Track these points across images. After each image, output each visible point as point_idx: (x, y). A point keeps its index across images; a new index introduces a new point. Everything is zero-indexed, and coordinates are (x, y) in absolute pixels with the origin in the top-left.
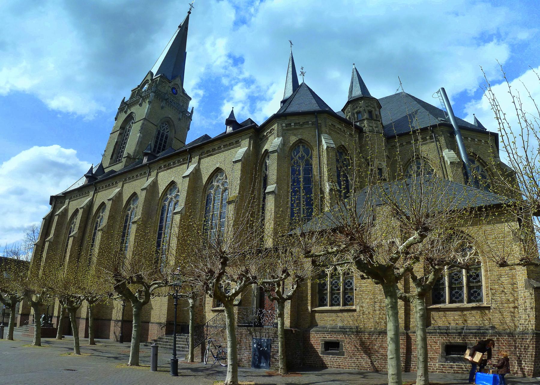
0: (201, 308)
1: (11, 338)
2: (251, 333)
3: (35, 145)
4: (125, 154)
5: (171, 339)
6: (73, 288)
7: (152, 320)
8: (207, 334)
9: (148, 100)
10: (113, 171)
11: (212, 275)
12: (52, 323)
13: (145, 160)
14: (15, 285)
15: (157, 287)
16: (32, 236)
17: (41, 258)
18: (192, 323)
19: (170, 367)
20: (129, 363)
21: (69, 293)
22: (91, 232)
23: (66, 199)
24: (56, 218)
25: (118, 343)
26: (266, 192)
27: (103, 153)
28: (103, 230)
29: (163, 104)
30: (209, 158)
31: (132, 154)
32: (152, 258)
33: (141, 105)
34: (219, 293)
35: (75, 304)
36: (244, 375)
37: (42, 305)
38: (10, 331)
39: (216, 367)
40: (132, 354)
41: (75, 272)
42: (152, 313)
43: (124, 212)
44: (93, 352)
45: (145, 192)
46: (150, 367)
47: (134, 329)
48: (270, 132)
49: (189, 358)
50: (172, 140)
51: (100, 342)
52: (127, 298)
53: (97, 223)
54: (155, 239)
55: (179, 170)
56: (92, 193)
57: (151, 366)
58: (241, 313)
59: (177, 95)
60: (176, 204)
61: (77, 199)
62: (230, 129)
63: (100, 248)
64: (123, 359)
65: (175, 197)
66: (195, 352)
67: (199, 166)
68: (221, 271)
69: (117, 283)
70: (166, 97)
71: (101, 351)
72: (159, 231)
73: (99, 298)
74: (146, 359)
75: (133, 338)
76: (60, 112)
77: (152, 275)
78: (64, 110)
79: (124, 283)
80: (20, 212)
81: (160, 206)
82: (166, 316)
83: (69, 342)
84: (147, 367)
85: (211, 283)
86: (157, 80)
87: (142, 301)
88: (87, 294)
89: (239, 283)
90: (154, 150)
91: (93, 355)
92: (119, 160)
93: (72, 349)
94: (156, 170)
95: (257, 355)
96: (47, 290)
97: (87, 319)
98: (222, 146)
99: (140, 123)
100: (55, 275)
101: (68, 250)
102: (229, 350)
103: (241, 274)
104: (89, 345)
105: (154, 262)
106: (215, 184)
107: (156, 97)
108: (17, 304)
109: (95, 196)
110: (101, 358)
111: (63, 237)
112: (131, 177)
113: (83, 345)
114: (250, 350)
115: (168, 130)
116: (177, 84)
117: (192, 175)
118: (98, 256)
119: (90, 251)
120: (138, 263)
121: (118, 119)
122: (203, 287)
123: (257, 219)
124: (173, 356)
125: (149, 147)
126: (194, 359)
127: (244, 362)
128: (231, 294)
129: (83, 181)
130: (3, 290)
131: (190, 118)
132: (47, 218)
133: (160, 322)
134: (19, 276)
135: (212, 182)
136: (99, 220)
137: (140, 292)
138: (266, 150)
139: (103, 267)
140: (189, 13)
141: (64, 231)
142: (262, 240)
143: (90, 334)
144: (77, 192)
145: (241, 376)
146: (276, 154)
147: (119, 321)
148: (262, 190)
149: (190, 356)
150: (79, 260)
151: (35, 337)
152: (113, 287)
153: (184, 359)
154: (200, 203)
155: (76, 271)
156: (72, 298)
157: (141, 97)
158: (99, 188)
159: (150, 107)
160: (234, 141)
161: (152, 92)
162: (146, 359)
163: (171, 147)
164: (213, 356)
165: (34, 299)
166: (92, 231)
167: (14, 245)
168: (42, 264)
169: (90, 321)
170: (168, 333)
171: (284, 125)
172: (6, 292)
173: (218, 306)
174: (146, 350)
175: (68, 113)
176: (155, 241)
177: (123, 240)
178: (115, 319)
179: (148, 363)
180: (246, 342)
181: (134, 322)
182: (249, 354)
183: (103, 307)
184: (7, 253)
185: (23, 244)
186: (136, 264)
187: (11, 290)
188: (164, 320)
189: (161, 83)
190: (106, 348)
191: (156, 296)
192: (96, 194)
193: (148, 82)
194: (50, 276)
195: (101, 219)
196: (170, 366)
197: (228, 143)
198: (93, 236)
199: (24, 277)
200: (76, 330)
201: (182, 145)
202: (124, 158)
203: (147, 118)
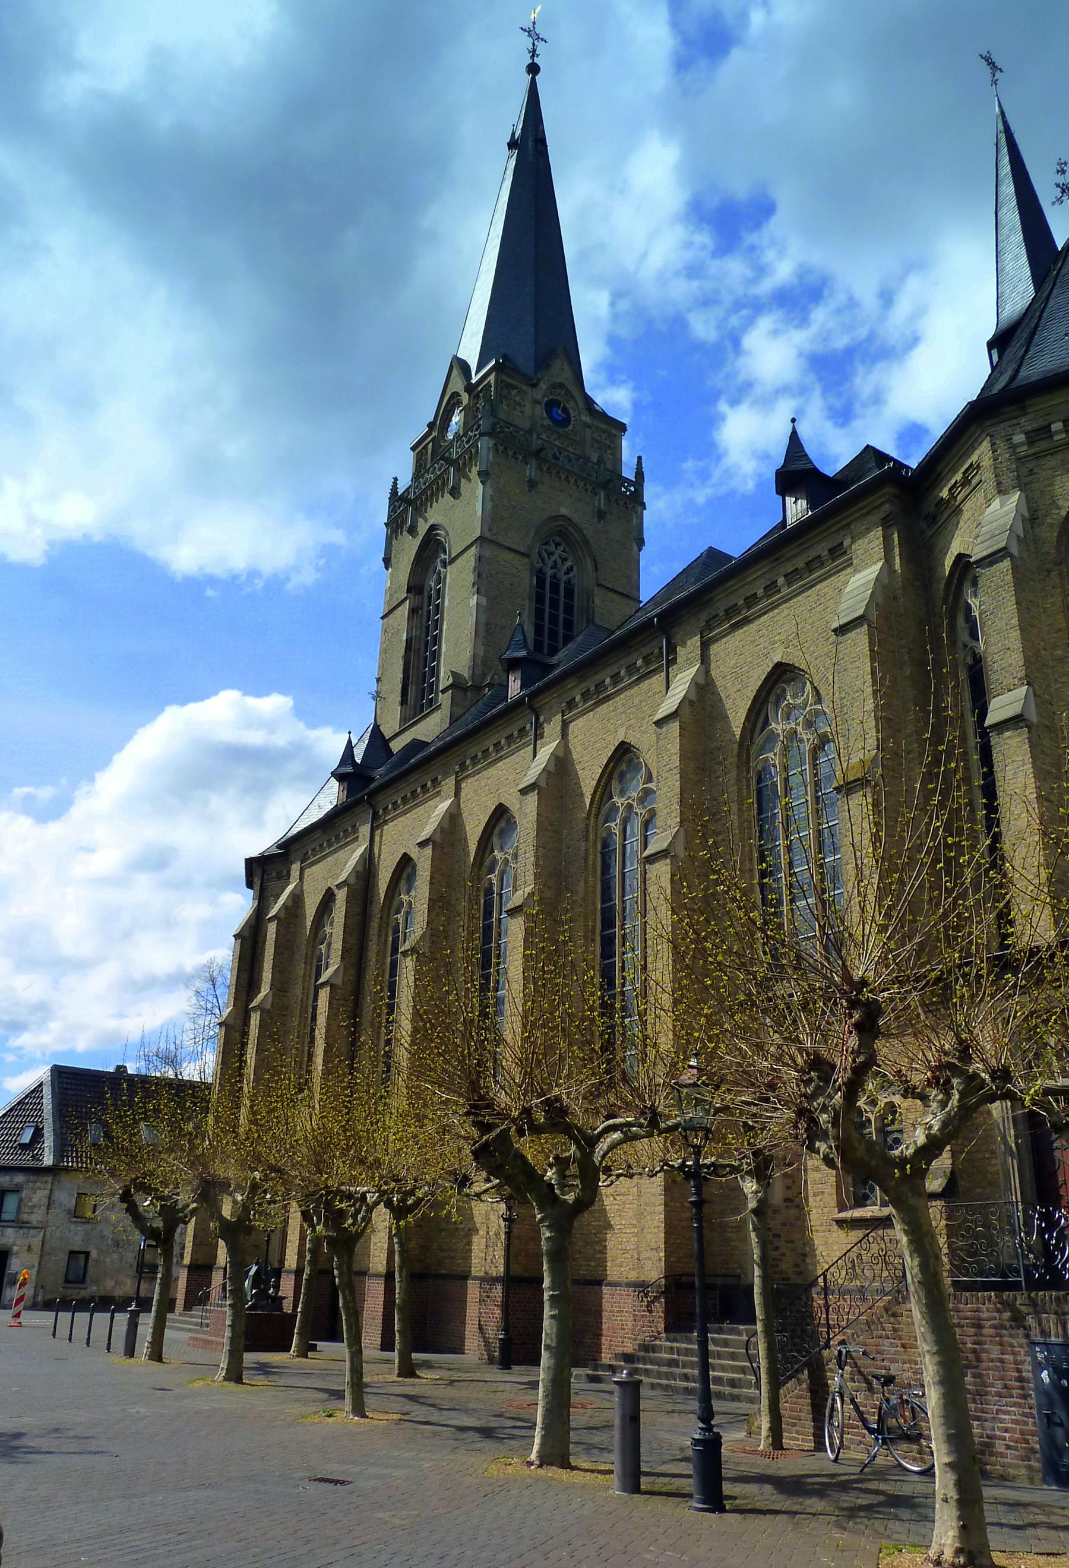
0: (793, 1212)
1: (156, 1355)
2: (1018, 1320)
3: (170, 702)
4: (444, 680)
5: (687, 1352)
6: (341, 1165)
7: (613, 1272)
8: (829, 1327)
9: (475, 470)
10: (417, 745)
11: (826, 1078)
12: (280, 1294)
13: (515, 687)
14: (174, 1165)
15: (621, 1142)
16: (210, 998)
17: (241, 1068)
18: (764, 1278)
19: (689, 1476)
20: (533, 1456)
21: (330, 1183)
22: (381, 962)
23: (292, 863)
24: (272, 928)
25: (495, 1369)
26: (988, 723)
27: (374, 687)
28: (418, 953)
29: (530, 471)
30: (740, 633)
31: (466, 674)
32: (592, 1034)
33: (455, 493)
34: (861, 1151)
35: (350, 1221)
36: (1012, 1519)
37: (250, 1230)
38: (155, 1328)
39: (881, 1474)
40: (545, 1417)
41: (346, 1107)
42: (610, 1244)
43: (477, 878)
44: (407, 1408)
45: (533, 798)
46: (611, 1472)
47: (547, 1312)
48: (966, 481)
49: (764, 1432)
50: (589, 596)
51: (432, 1367)
52: (517, 1189)
53: (396, 930)
54: (593, 960)
55: (636, 701)
56: (365, 830)
57: (616, 1467)
58: (959, 1226)
59: (571, 427)
60: (647, 825)
61: (324, 857)
62: (797, 509)
63: (416, 1014)
64: (512, 1437)
65: (642, 801)
66: (784, 1406)
67: (707, 672)
68: (861, 1059)
69: (481, 1137)
70: (536, 443)
71: (436, 1402)
72: (603, 930)
73: (426, 1194)
74: (597, 1438)
75: (548, 1347)
76: (211, 581)
77: (599, 1095)
78: (219, 571)
79: (504, 1136)
80: (168, 923)
81: (595, 841)
82: (662, 1254)
83: (331, 1365)
84: (600, 1472)
85: (824, 1109)
86: (489, 385)
87: (570, 1197)
88: (386, 1183)
89: (939, 1102)
90: (538, 645)
91: (406, 1417)
92: (431, 702)
93: (339, 1395)
94: (557, 713)
95: (1061, 1425)
96: (266, 1175)
97: (389, 1277)
98: (781, 581)
99: (469, 560)
100: (287, 1124)
101: (317, 1031)
102: (933, 1399)
103: (941, 1067)
104: (395, 1378)
105: (601, 1048)
106: (778, 727)
107: (501, 448)
108: (178, 1230)
109: (377, 838)
110: (435, 1434)
111: (298, 991)
112: (480, 754)
113: (375, 1379)
114: (1025, 1397)
115: (569, 564)
116: (561, 385)
117: (687, 709)
118: (413, 1043)
119: (386, 1027)
120: (545, 1055)
121: (393, 560)
122: (796, 1127)
123: (974, 837)
124: (701, 1425)
125: (519, 637)
126: (785, 1434)
127: (1003, 1455)
128: (911, 1151)
129: (331, 796)
130: (140, 1183)
131: (636, 501)
132: (246, 934)
133: (642, 1278)
134: (184, 1135)
135: (766, 723)
136: (400, 917)
137: (561, 1163)
138: (960, 557)
139: (430, 1082)
140: (533, 69)
141: (300, 968)
142: (1004, 918)
143: (397, 1335)
144: (318, 834)
145: (1001, 1525)
146: (1006, 563)
147: (494, 1280)
148: (971, 719)
149: (765, 1423)
150: (353, 1063)
151: (227, 1348)
152: (467, 1151)
153: (743, 1435)
154: (734, 808)
155: (349, 1102)
156: (341, 1202)
157: (450, 462)
158: (385, 809)
159: (490, 491)
160: (822, 549)
161: (481, 435)
162: (597, 1438)
163: (590, 621)
164: (864, 1421)
165: (227, 1211)
166: (385, 956)
167: (164, 1034)
168: (245, 1089)
169: (397, 1285)
170: (676, 1324)
171: (1019, 438)
172: (147, 1190)
173: (861, 1201)
174: (597, 1400)
175: (235, 577)
176: (593, 968)
177: (486, 978)
178: (482, 1274)
179: (606, 1455)
180: (1002, 1361)
181: (546, 1284)
182: (1024, 1414)
183: (441, 1230)
184: (148, 1059)
185: (189, 1025)
186: (539, 1062)
187: (161, 1182)
188: (654, 1271)
189: (504, 392)
190: (451, 1392)
191: (621, 1175)
192: (378, 832)
193: (459, 403)
194: (270, 1129)
195: (408, 913)
196: (688, 1468)
197: (800, 563)
198: (391, 977)
199: (196, 1137)
200: (353, 1319)
201: (629, 608)
202: (444, 691)
203: (488, 535)
